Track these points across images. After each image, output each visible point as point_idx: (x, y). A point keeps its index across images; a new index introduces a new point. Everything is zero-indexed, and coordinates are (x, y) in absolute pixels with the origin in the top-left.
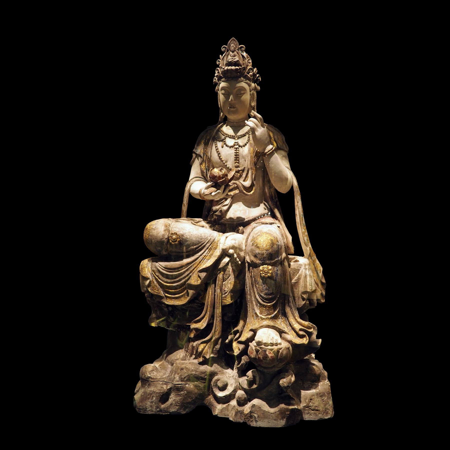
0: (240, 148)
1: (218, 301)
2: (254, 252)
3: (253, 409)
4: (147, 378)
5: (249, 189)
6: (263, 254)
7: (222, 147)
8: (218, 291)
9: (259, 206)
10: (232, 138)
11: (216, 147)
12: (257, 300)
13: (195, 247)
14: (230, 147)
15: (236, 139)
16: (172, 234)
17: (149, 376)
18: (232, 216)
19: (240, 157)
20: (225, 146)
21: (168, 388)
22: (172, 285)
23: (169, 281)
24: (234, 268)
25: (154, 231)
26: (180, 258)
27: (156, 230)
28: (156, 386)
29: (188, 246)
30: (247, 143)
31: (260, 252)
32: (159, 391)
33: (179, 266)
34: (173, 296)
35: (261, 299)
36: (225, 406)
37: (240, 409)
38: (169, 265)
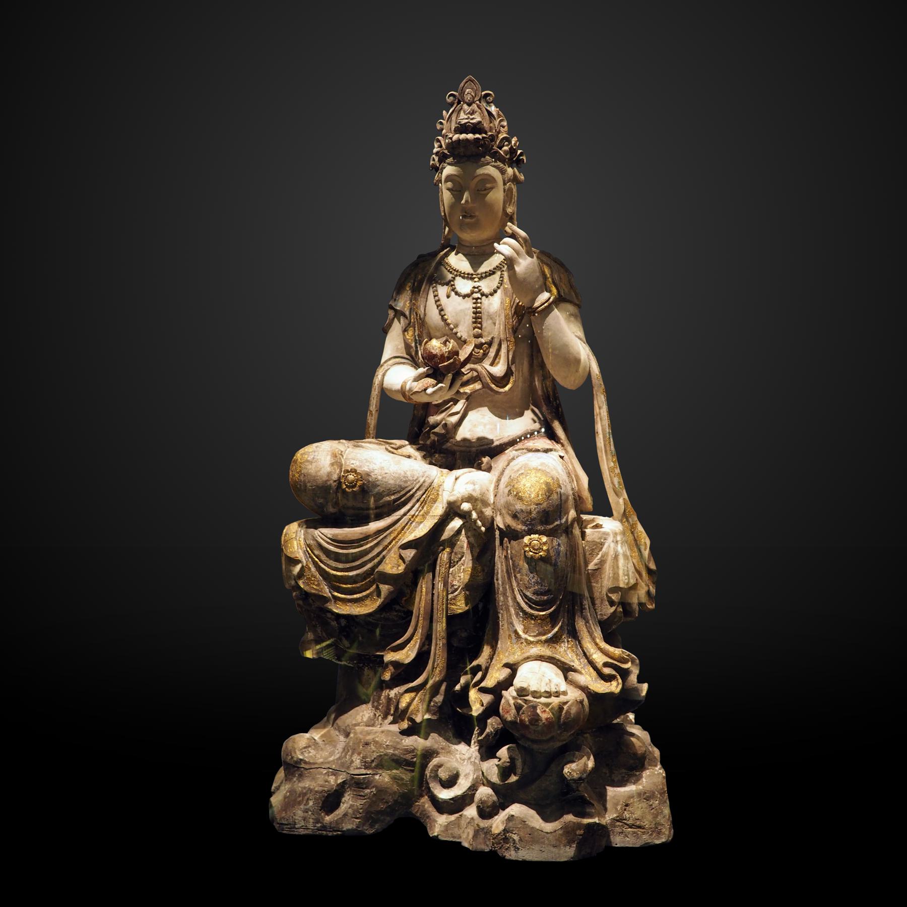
0: (484, 298)
1: (439, 606)
2: (512, 508)
3: (511, 824)
4: (296, 762)
5: (502, 381)
6: (530, 513)
7: (448, 297)
8: (440, 586)
9: (521, 414)
10: (467, 278)
11: (435, 296)
12: (518, 604)
13: (393, 497)
14: (464, 296)
15: (476, 280)
16: (347, 471)
17: (301, 757)
18: (468, 435)
19: (484, 317)
20: (453, 293)
21: (339, 781)
22: (346, 574)
23: (341, 566)
24: (472, 539)
25: (310, 467)
26: (363, 520)
27: (314, 465)
28: (314, 779)
29: (380, 496)
30: (498, 288)
31: (524, 508)
32: (321, 789)
33: (361, 536)
34: (349, 597)
35: (526, 603)
36: (453, 818)
37: (484, 824)
38: (341, 534)
